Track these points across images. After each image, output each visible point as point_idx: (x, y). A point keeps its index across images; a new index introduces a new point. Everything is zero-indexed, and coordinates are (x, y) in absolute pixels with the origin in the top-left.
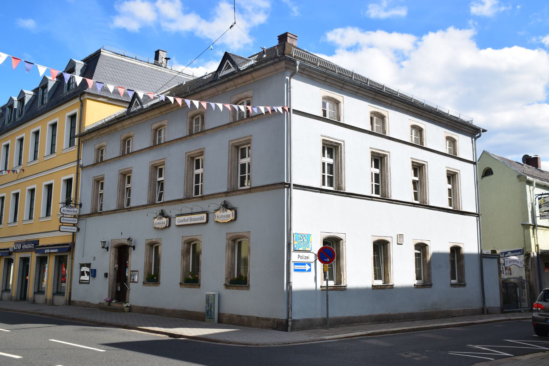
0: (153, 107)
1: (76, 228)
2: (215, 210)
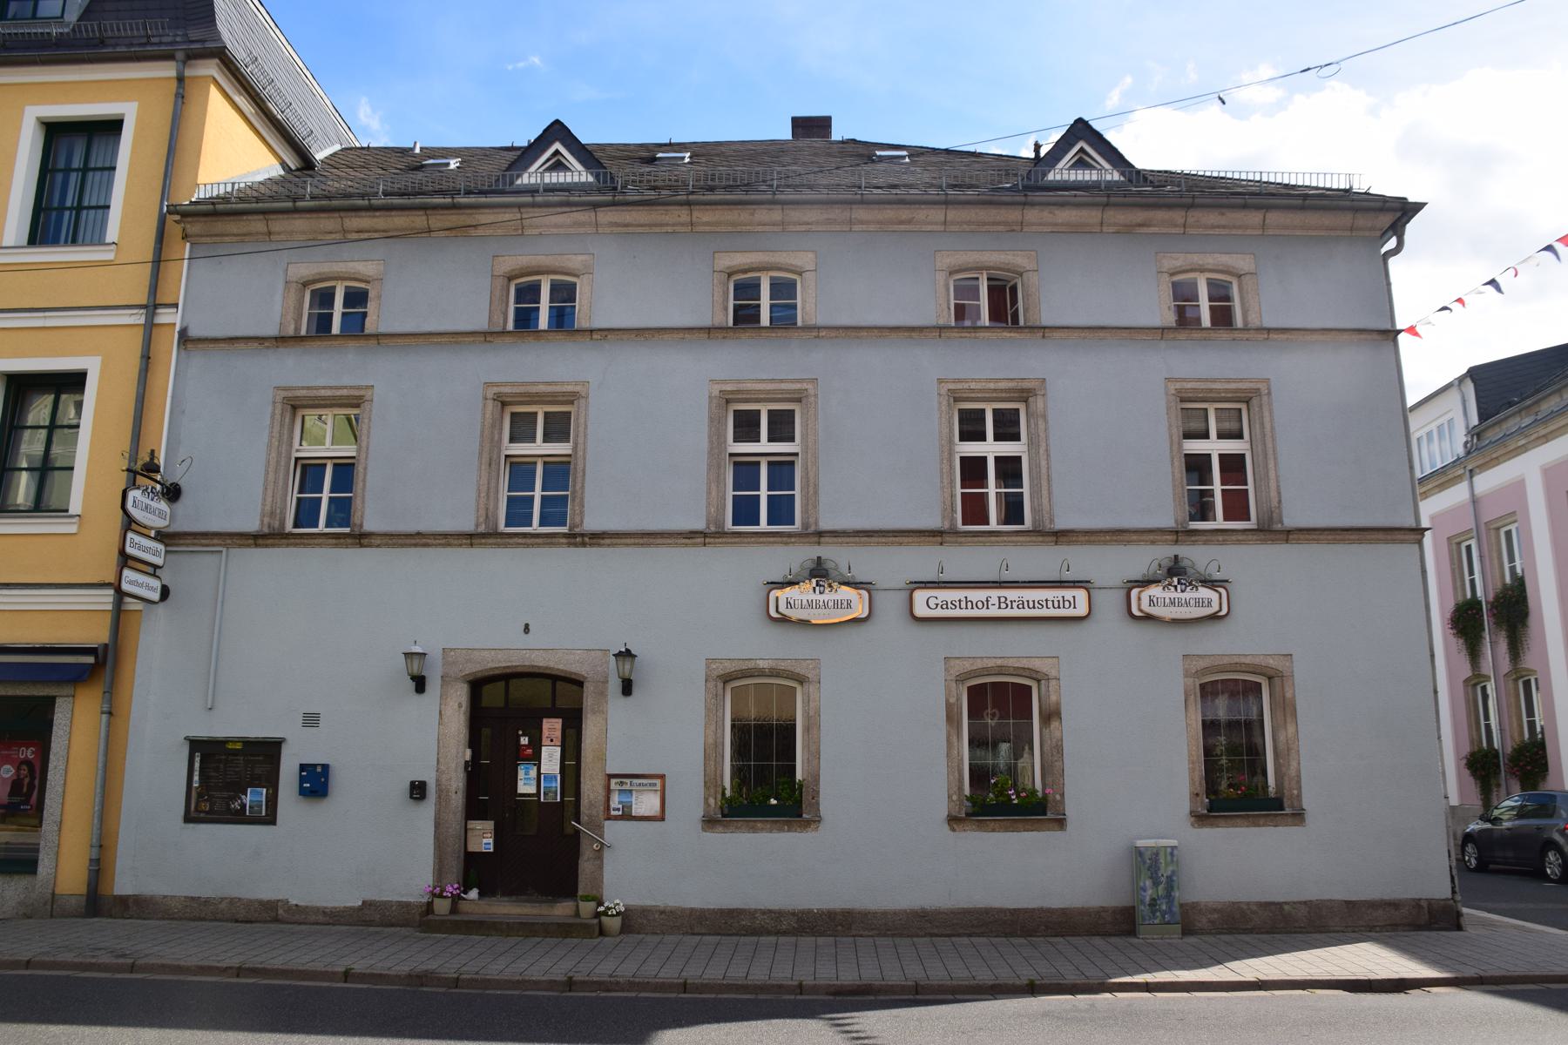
0: (372, 201)
1: (156, 584)
2: (911, 583)
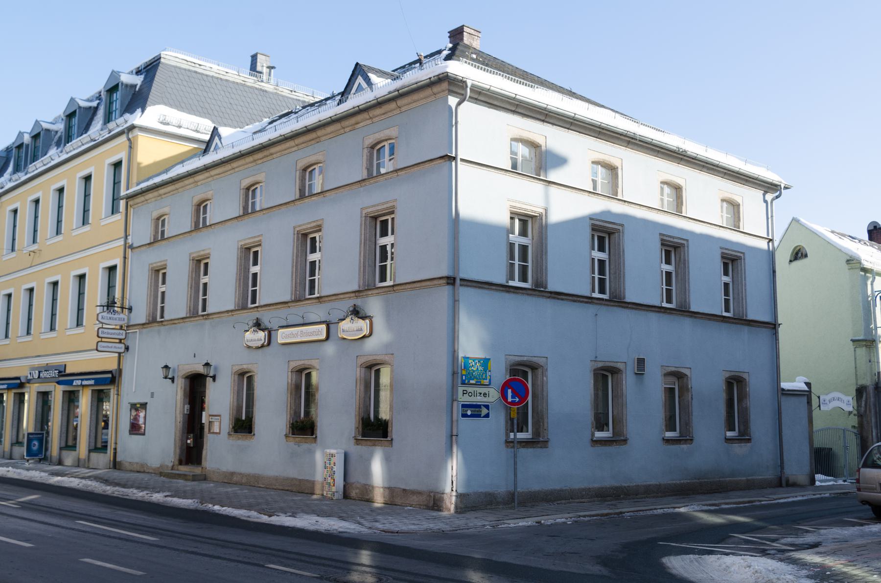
1: (123, 346)
